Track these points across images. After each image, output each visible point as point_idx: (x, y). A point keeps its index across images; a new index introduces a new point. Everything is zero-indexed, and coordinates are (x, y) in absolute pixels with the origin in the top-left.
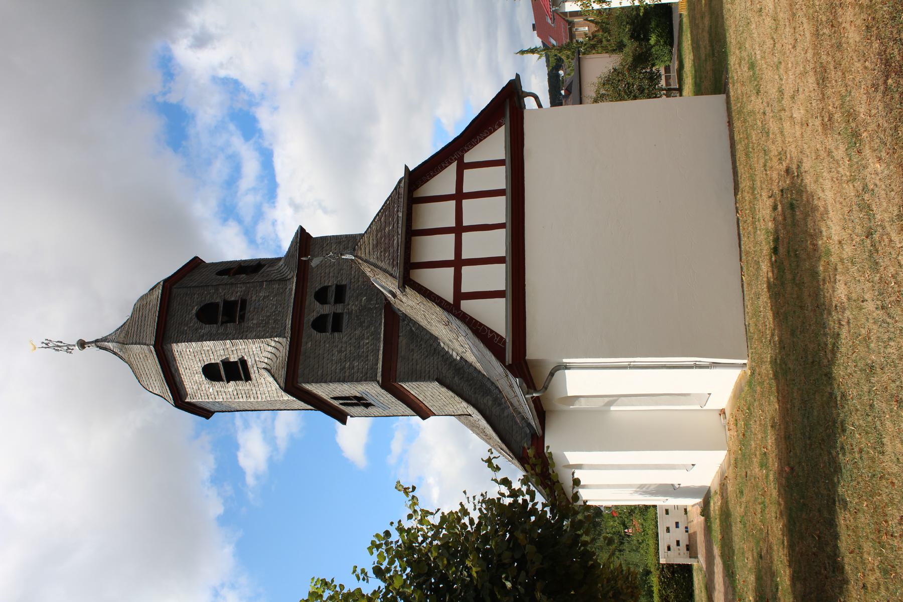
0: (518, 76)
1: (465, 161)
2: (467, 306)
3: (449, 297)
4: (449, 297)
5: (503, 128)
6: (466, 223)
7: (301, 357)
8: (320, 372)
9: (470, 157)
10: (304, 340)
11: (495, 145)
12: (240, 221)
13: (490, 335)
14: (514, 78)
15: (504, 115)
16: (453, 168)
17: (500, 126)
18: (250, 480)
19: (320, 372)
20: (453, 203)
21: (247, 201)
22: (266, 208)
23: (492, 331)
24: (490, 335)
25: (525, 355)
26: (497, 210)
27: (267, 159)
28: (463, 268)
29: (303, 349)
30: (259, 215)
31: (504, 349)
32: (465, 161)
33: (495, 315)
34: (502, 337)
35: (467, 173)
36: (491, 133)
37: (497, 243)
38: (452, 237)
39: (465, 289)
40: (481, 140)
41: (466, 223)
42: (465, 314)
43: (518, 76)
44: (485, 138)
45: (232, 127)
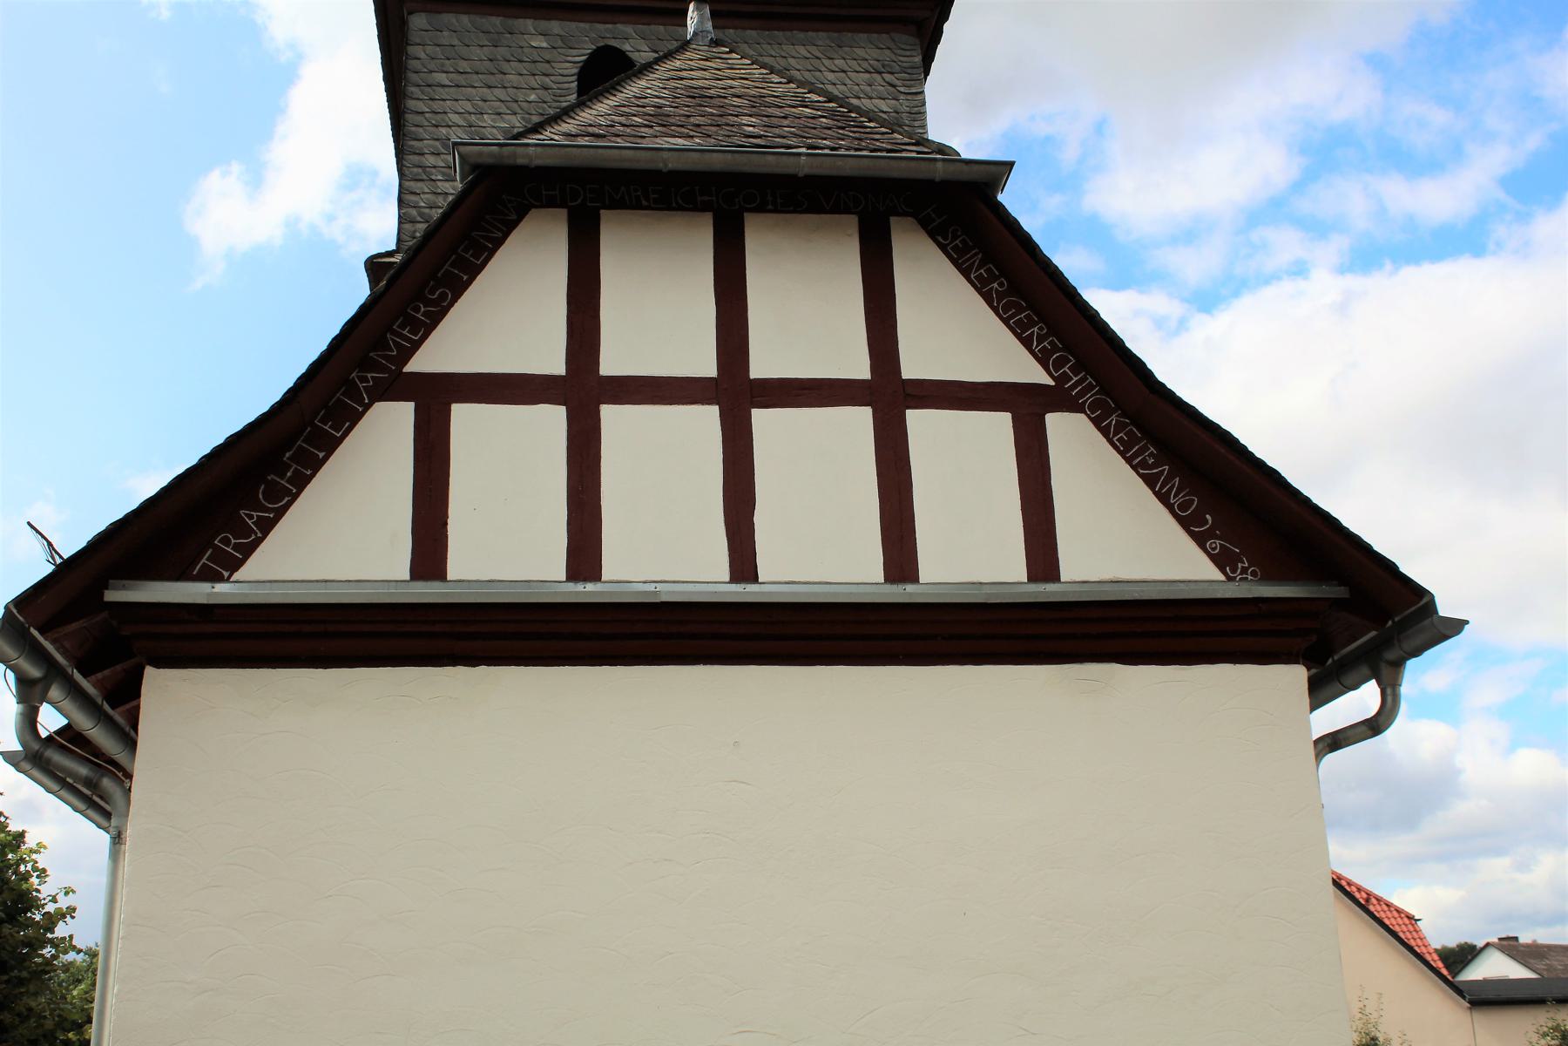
0: (1455, 627)
1: (1052, 420)
2: (389, 428)
3: (438, 354)
4: (438, 354)
5: (1210, 572)
6: (764, 420)
7: (497, 21)
8: (442, 78)
9: (1072, 439)
10: (555, 26)
11: (1122, 536)
12: (1299, 186)
13: (250, 517)
14: (1445, 609)
15: (1267, 577)
16: (1026, 370)
17: (1219, 561)
18: (1314, 671)
19: (442, 78)
20: (860, 368)
21: (1353, 198)
22: (1337, 246)
23: (267, 526)
24: (250, 517)
25: (161, 663)
26: (819, 541)
27: (1462, 240)
28: (561, 411)
29: (529, 24)
30: (1317, 229)
31: (183, 575)
32: (1052, 420)
33: (341, 534)
34: (236, 565)
35: (998, 427)
36: (1185, 523)
37: (663, 541)
38: (705, 365)
39: (465, 418)
40: (1150, 481)
41: (764, 420)
42: (356, 418)
43: (1455, 627)
44: (1163, 498)
45: (1534, 141)
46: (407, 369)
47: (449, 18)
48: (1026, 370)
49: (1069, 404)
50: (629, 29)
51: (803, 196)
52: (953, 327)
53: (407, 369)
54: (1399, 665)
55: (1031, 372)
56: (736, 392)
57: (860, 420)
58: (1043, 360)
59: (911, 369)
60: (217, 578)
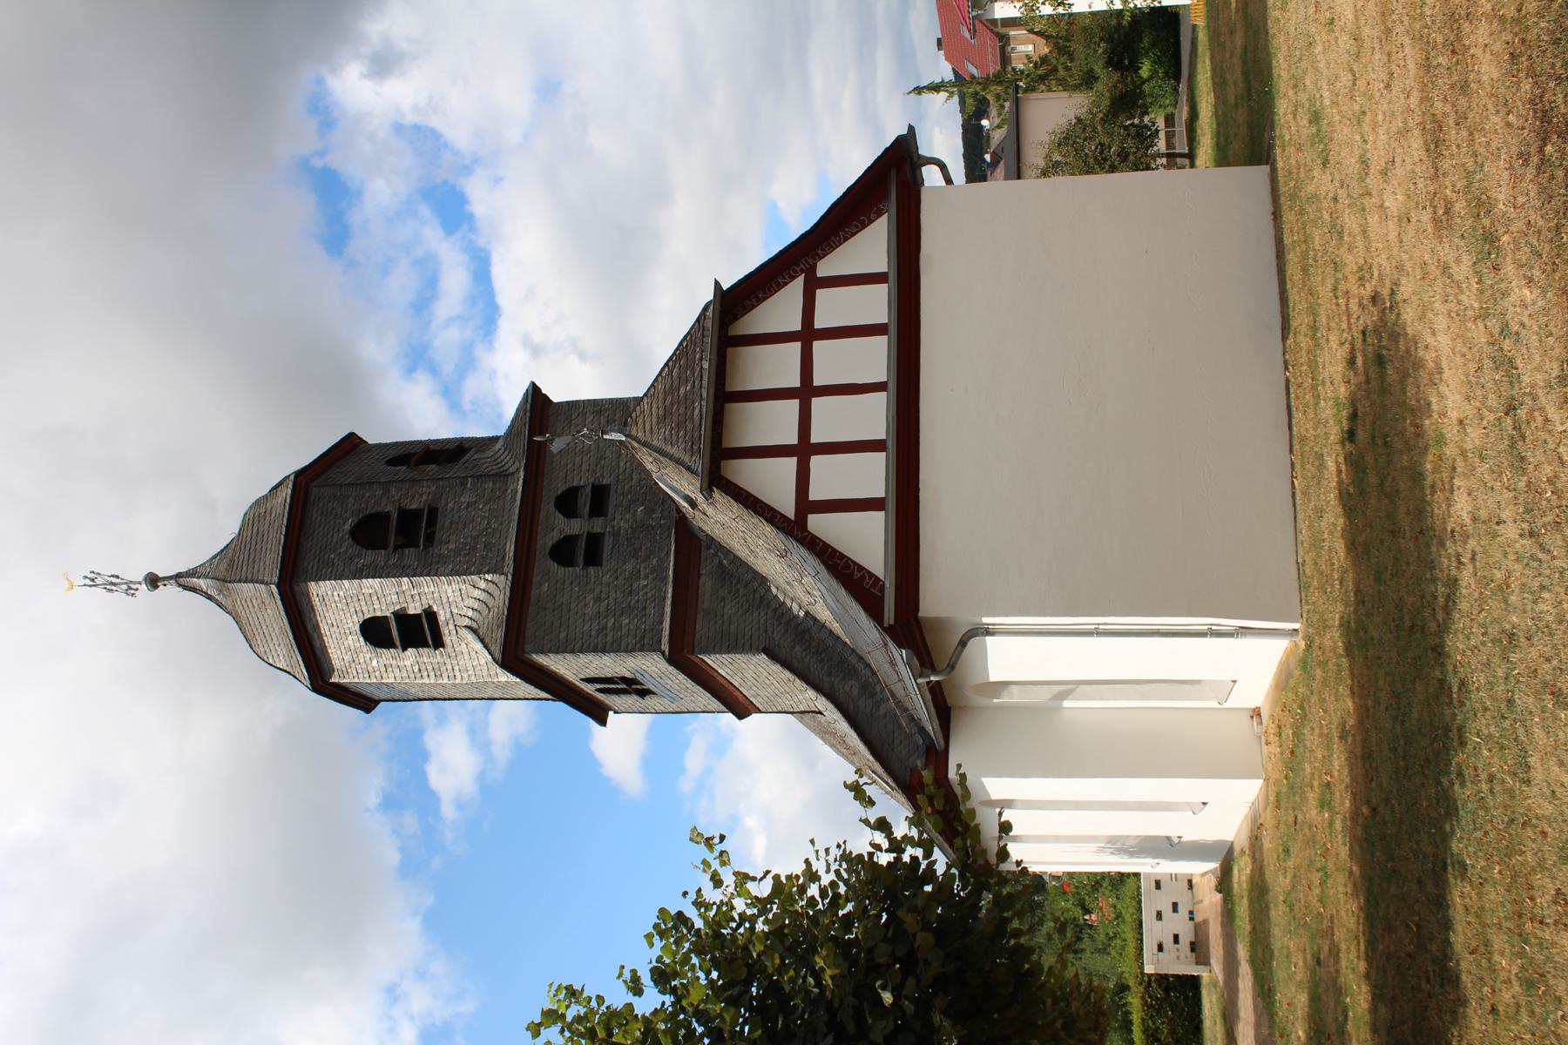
3: (788, 507)
4: (788, 507)
8: (562, 636)
9: (825, 268)
10: (536, 579)
11: (870, 248)
12: (434, 371)
13: (857, 575)
15: (886, 197)
16: (798, 285)
17: (880, 215)
18: (448, 811)
19: (562, 636)
20: (796, 347)
23: (861, 568)
24: (857, 575)
26: (871, 359)
29: (534, 593)
30: (468, 362)
31: (882, 599)
33: (866, 540)
34: (877, 579)
35: (822, 295)
36: (864, 227)
37: (871, 417)
38: (793, 405)
39: (815, 494)
40: (846, 239)
43: (911, 129)
44: (853, 234)
46: (792, 516)
47: (528, 633)
48: (798, 285)
49: (813, 268)
50: (539, 544)
51: (721, 370)
52: (782, 310)
53: (792, 516)
54: (920, 156)
55: (799, 282)
56: (806, 392)
57: (818, 346)
58: (793, 278)
59: (796, 326)
60: (883, 587)
